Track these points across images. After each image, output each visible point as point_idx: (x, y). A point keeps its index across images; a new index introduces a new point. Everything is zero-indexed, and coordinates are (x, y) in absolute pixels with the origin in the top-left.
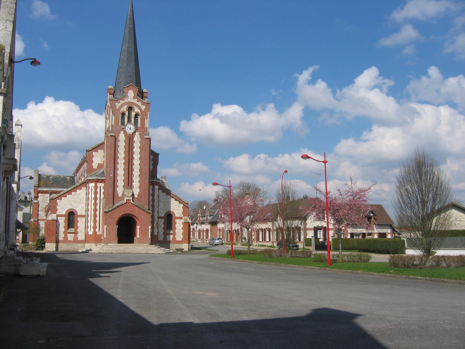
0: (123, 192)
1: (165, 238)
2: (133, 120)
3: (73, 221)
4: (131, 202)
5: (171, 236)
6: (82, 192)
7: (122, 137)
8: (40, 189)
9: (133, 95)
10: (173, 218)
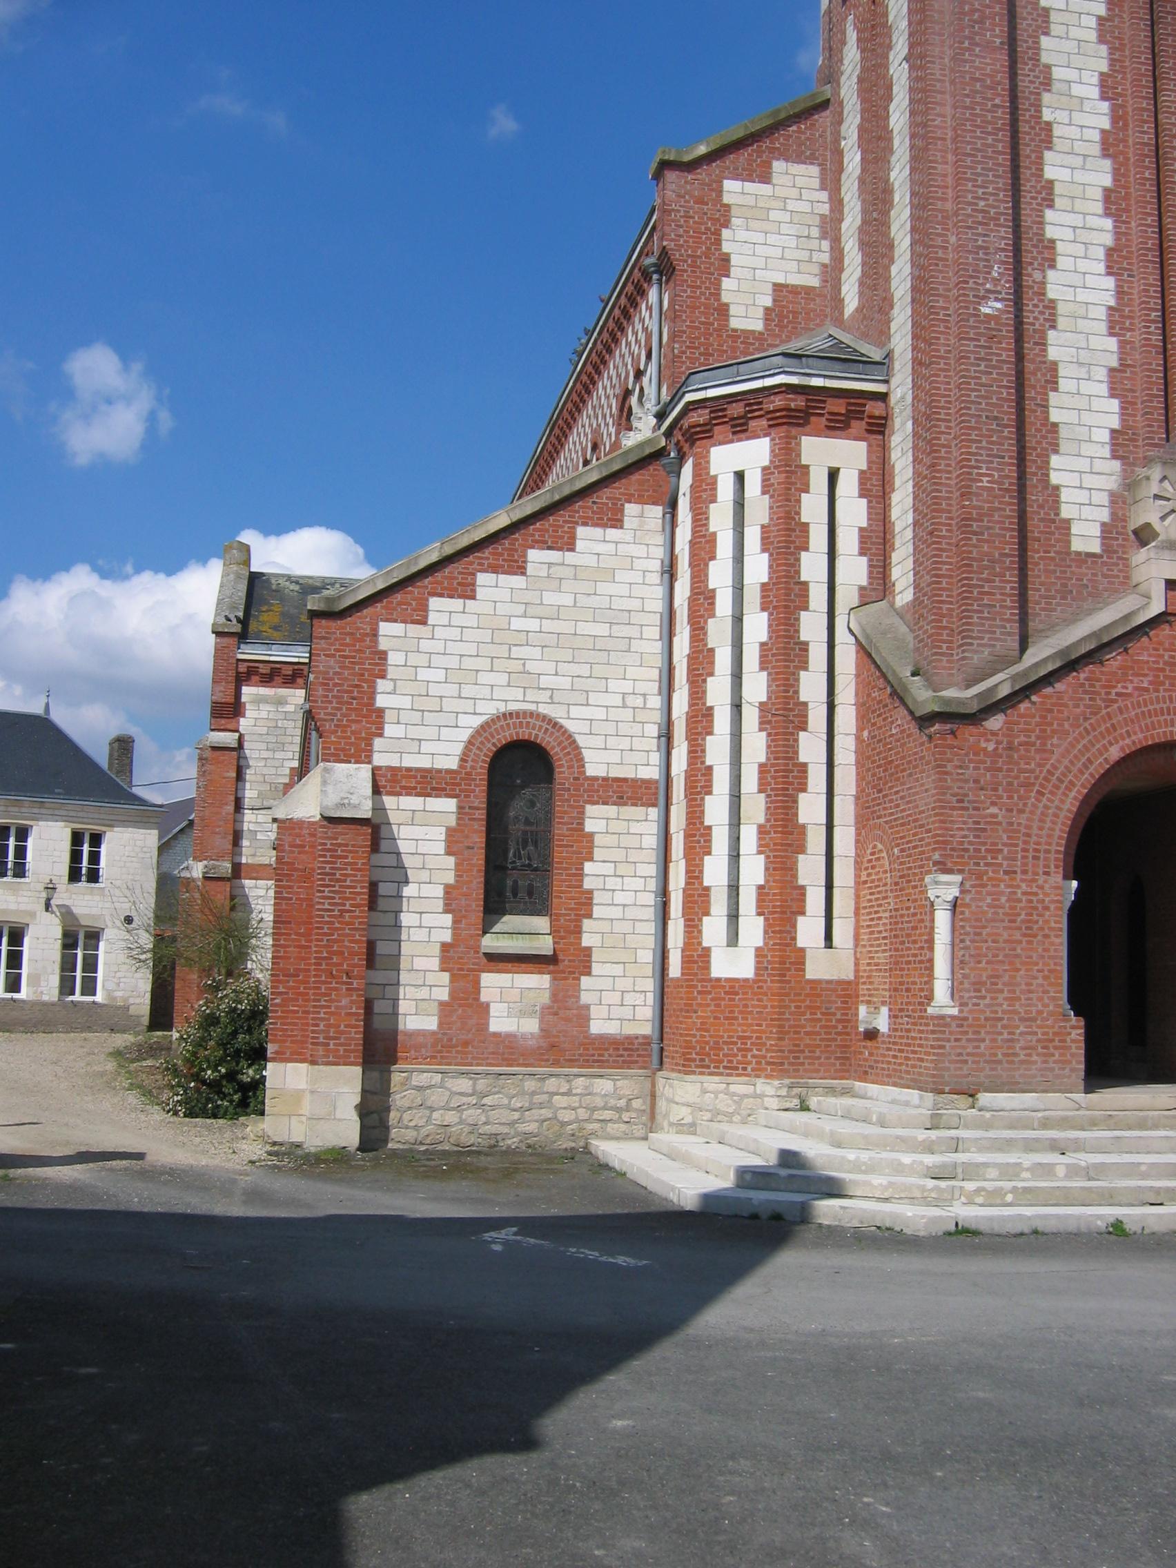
0: (1120, 502)
3: (539, 838)
6: (621, 556)
8: (250, 653)
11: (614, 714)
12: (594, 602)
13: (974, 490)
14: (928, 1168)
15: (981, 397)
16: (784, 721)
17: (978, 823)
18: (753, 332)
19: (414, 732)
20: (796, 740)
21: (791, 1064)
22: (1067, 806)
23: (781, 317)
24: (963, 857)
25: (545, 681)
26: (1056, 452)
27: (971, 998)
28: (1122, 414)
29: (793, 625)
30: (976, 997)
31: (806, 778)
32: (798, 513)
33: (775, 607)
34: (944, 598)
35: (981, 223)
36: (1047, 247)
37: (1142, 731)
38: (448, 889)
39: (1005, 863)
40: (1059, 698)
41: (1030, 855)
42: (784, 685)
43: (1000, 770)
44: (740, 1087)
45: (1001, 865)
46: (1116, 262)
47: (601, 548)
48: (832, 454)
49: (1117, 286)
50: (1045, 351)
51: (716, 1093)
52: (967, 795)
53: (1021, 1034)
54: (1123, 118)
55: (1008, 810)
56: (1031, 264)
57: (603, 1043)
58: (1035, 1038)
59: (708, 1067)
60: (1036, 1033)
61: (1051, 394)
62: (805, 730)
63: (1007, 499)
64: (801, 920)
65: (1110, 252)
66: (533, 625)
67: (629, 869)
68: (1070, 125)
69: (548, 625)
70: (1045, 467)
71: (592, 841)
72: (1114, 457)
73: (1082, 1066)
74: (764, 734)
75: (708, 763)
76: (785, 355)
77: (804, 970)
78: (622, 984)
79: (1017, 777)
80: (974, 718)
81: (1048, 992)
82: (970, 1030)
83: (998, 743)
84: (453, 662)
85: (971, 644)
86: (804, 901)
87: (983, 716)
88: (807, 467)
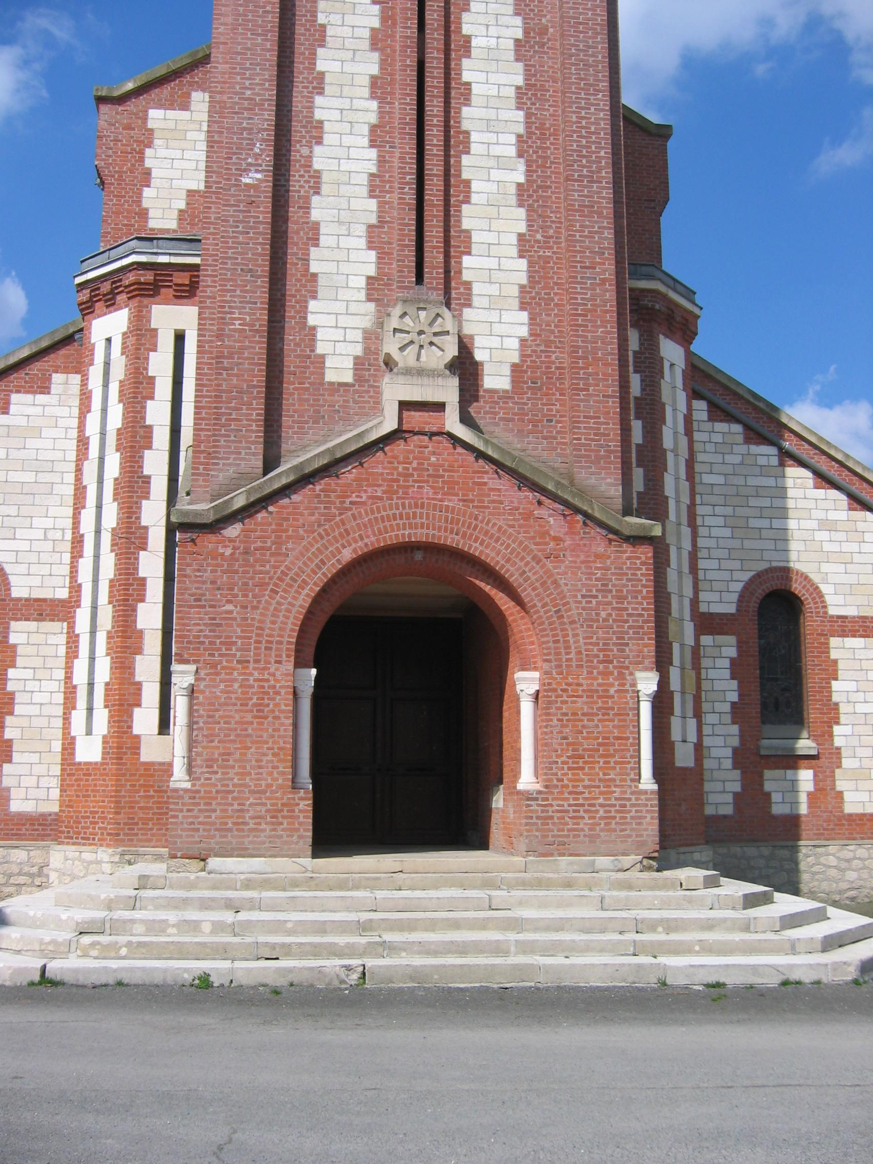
0: (372, 338)
1: (752, 797)
4: (452, 423)
5: (806, 777)
10: (810, 625)
11: (36, 546)
12: (22, 454)
13: (227, 332)
14: (77, 923)
15: (238, 253)
16: (127, 543)
17: (214, 619)
20: (137, 559)
21: (125, 834)
23: (193, 217)
24: (199, 649)
27: (202, 773)
28: (379, 263)
29: (138, 462)
30: (207, 772)
31: (145, 590)
32: (146, 369)
33: (125, 448)
34: (203, 427)
35: (246, 109)
36: (316, 127)
37: (374, 535)
39: (239, 654)
40: (295, 508)
41: (263, 646)
42: (128, 513)
43: (237, 572)
44: (88, 855)
45: (235, 655)
46: (380, 136)
47: (31, 410)
48: (171, 317)
49: (379, 156)
50: (309, 213)
51: (73, 860)
52: (204, 595)
53: (251, 805)
54: (393, 18)
55: (242, 607)
56: (300, 142)
57: (22, 820)
58: (264, 809)
59: (72, 838)
60: (265, 804)
61: (312, 249)
62: (145, 549)
63: (257, 339)
64: (137, 711)
65: (373, 129)
68: (343, 25)
70: (303, 311)
71: (15, 652)
72: (369, 299)
73: (310, 834)
74: (113, 554)
75: (79, 582)
76: (137, 238)
77: (139, 754)
78: (37, 770)
79: (252, 578)
80: (215, 526)
81: (278, 767)
82: (202, 802)
83: (234, 548)
85: (217, 464)
86: (140, 695)
87: (222, 525)
88: (156, 330)
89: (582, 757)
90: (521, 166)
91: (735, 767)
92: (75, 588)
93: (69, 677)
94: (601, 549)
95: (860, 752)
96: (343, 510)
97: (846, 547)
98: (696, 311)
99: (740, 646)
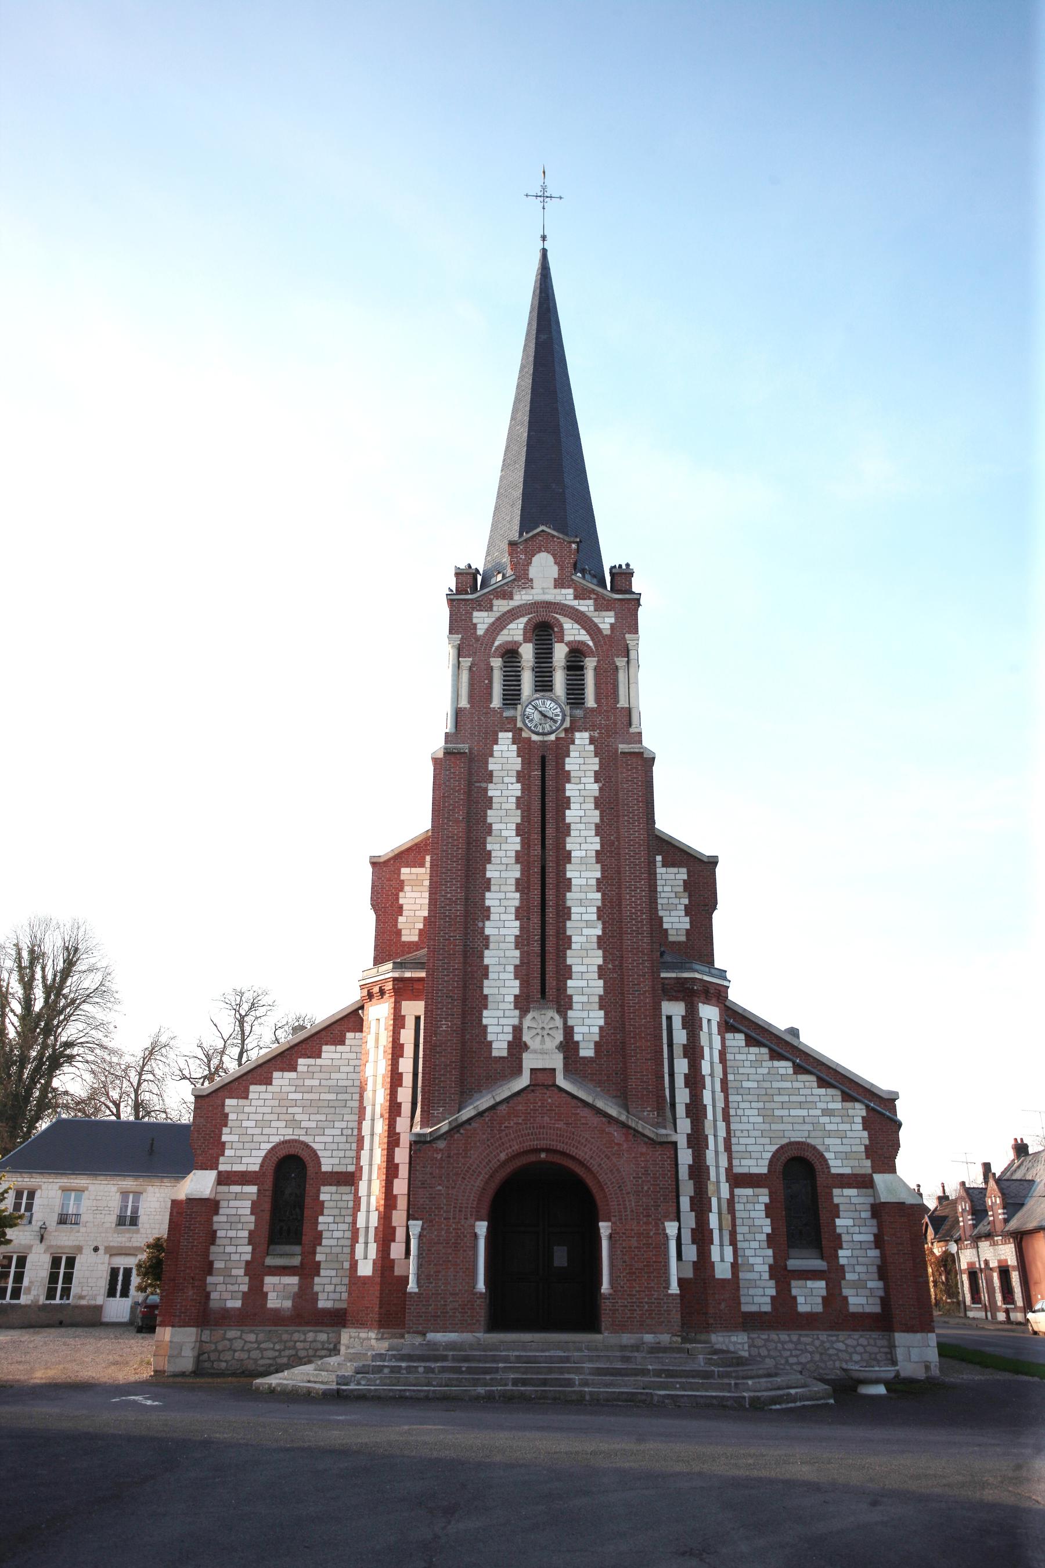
0: (517, 1030)
2: (559, 679)
3: (299, 1203)
7: (505, 757)
9: (554, 571)
11: (337, 1139)
18: (412, 942)
19: (239, 1153)
22: (477, 1184)
25: (303, 1124)
26: (486, 1008)
38: (251, 1233)
66: (299, 1096)
67: (341, 1219)
69: (306, 1096)
78: (334, 1280)
84: (259, 1117)
89: (635, 1273)
90: (600, 925)
91: (771, 1278)
92: (360, 1169)
93: (354, 1222)
94: (644, 1150)
95: (858, 1268)
96: (500, 1131)
97: (842, 1127)
98: (726, 983)
99: (771, 1196)
